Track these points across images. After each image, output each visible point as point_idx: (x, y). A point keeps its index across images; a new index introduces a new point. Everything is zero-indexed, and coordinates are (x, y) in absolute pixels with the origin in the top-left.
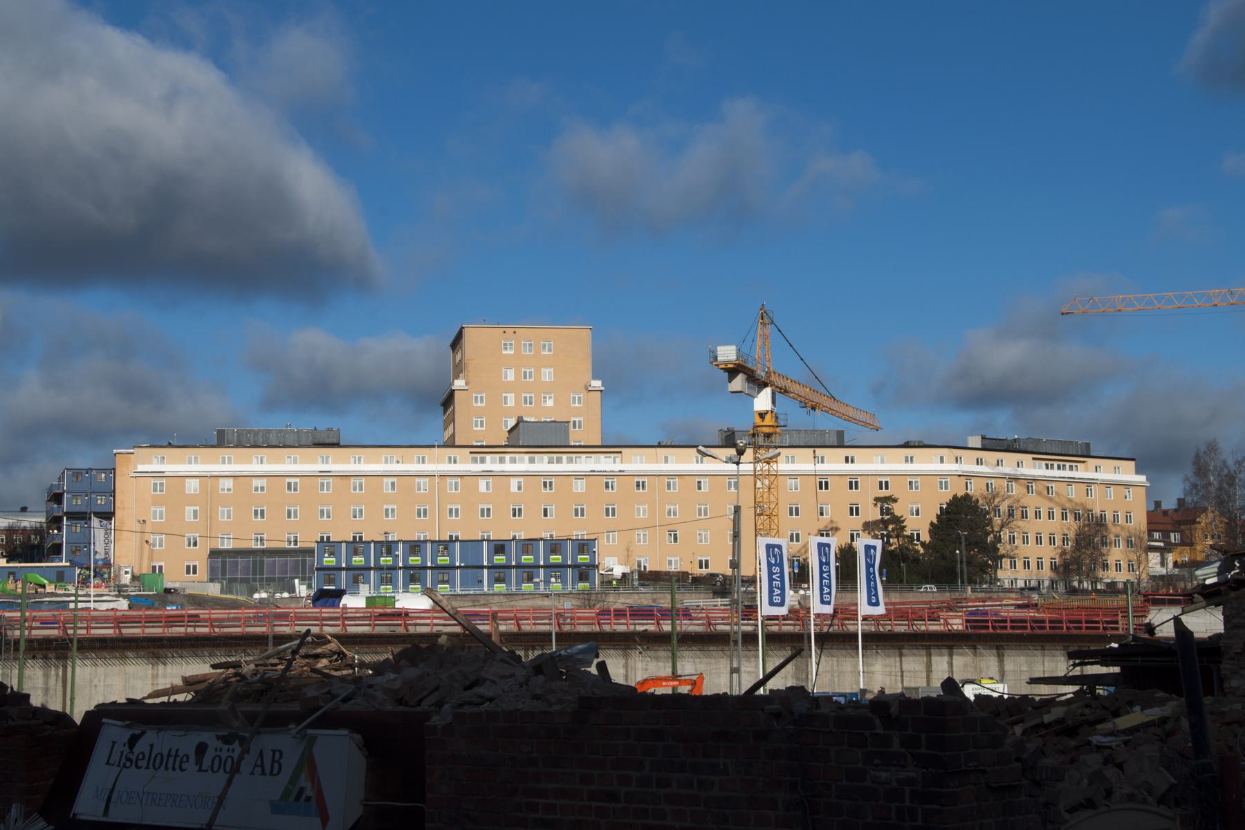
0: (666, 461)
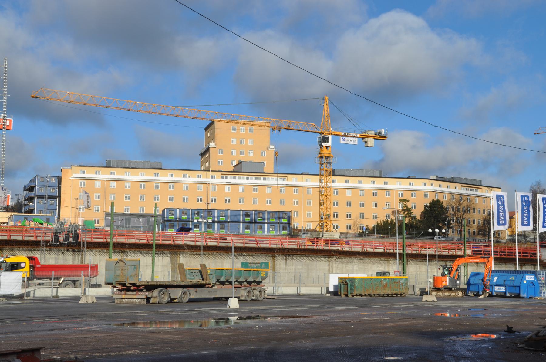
0: (307, 181)
